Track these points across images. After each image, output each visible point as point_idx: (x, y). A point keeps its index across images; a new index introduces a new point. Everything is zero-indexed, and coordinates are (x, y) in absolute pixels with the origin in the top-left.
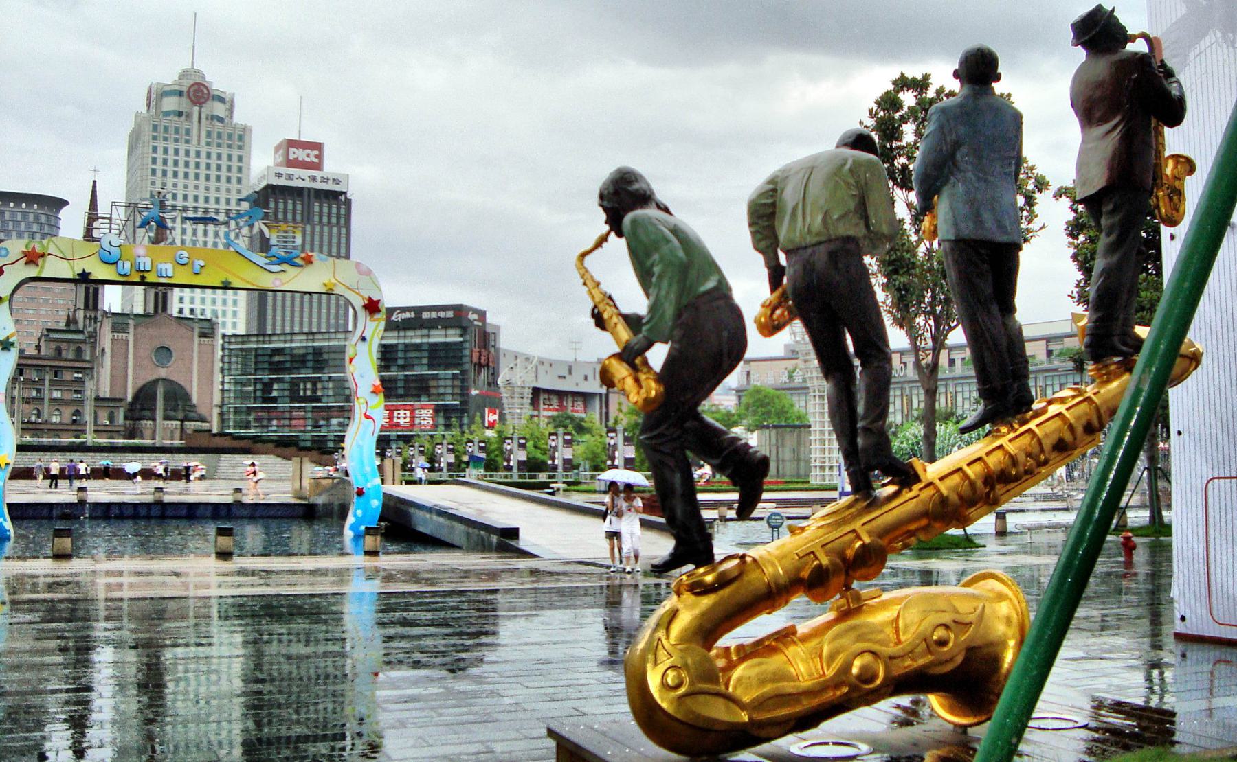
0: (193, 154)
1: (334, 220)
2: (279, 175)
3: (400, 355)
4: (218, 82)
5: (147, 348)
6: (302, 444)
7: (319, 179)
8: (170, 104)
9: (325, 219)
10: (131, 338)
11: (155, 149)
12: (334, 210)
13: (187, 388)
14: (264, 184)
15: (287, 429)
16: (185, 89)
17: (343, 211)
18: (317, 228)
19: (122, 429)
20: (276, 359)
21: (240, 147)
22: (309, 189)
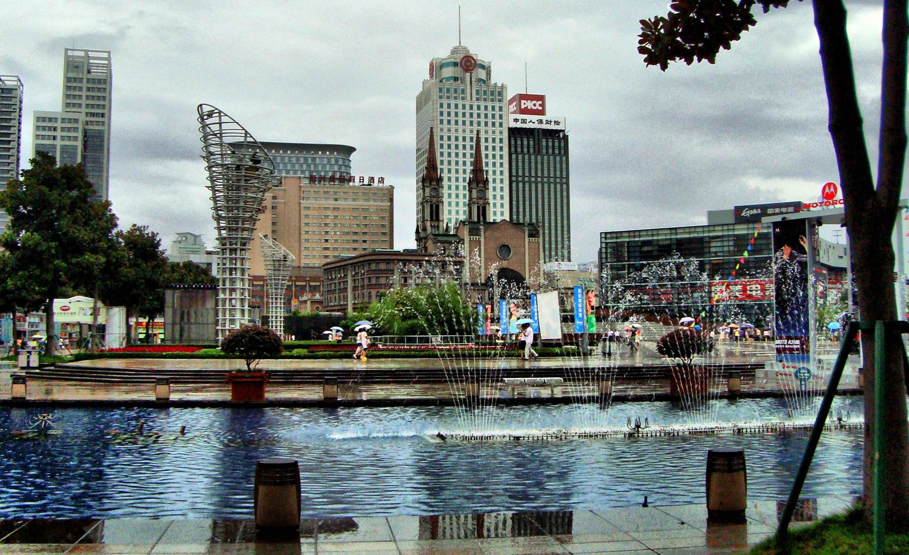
0: (468, 107)
1: (557, 151)
4: (481, 55)
8: (448, 72)
9: (550, 151)
10: (482, 240)
11: (441, 106)
12: (557, 144)
16: (458, 61)
17: (562, 144)
18: (546, 158)
20: (646, 249)
21: (500, 101)
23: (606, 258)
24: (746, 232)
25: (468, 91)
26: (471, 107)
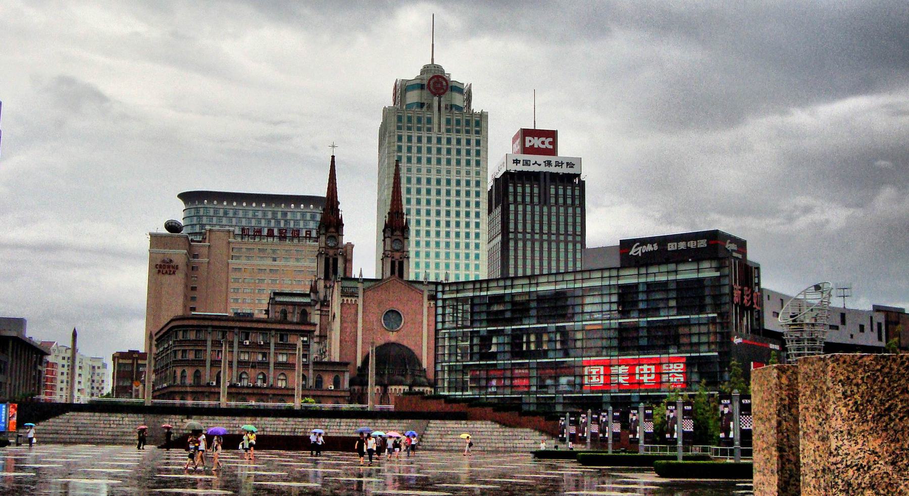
0: (434, 140)
1: (569, 201)
2: (516, 162)
3: (642, 297)
4: (456, 75)
5: (377, 315)
6: (525, 408)
7: (553, 164)
8: (413, 97)
9: (561, 201)
10: (360, 302)
11: (400, 139)
12: (569, 192)
13: (417, 352)
14: (503, 170)
15: (508, 391)
16: (425, 82)
17: (577, 193)
18: (554, 209)
19: (348, 394)
20: (495, 308)
21: (477, 132)
22: (545, 173)
23: (443, 322)
24: (635, 281)
25: (436, 120)
26: (439, 140)
